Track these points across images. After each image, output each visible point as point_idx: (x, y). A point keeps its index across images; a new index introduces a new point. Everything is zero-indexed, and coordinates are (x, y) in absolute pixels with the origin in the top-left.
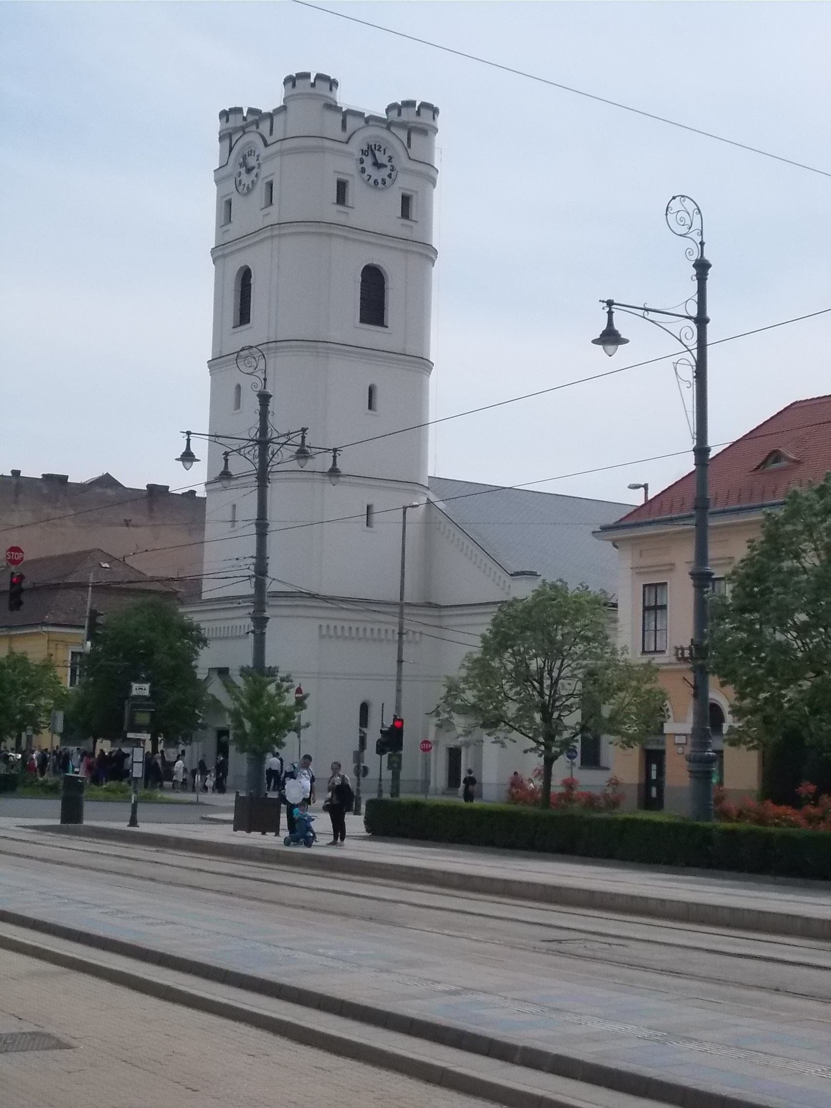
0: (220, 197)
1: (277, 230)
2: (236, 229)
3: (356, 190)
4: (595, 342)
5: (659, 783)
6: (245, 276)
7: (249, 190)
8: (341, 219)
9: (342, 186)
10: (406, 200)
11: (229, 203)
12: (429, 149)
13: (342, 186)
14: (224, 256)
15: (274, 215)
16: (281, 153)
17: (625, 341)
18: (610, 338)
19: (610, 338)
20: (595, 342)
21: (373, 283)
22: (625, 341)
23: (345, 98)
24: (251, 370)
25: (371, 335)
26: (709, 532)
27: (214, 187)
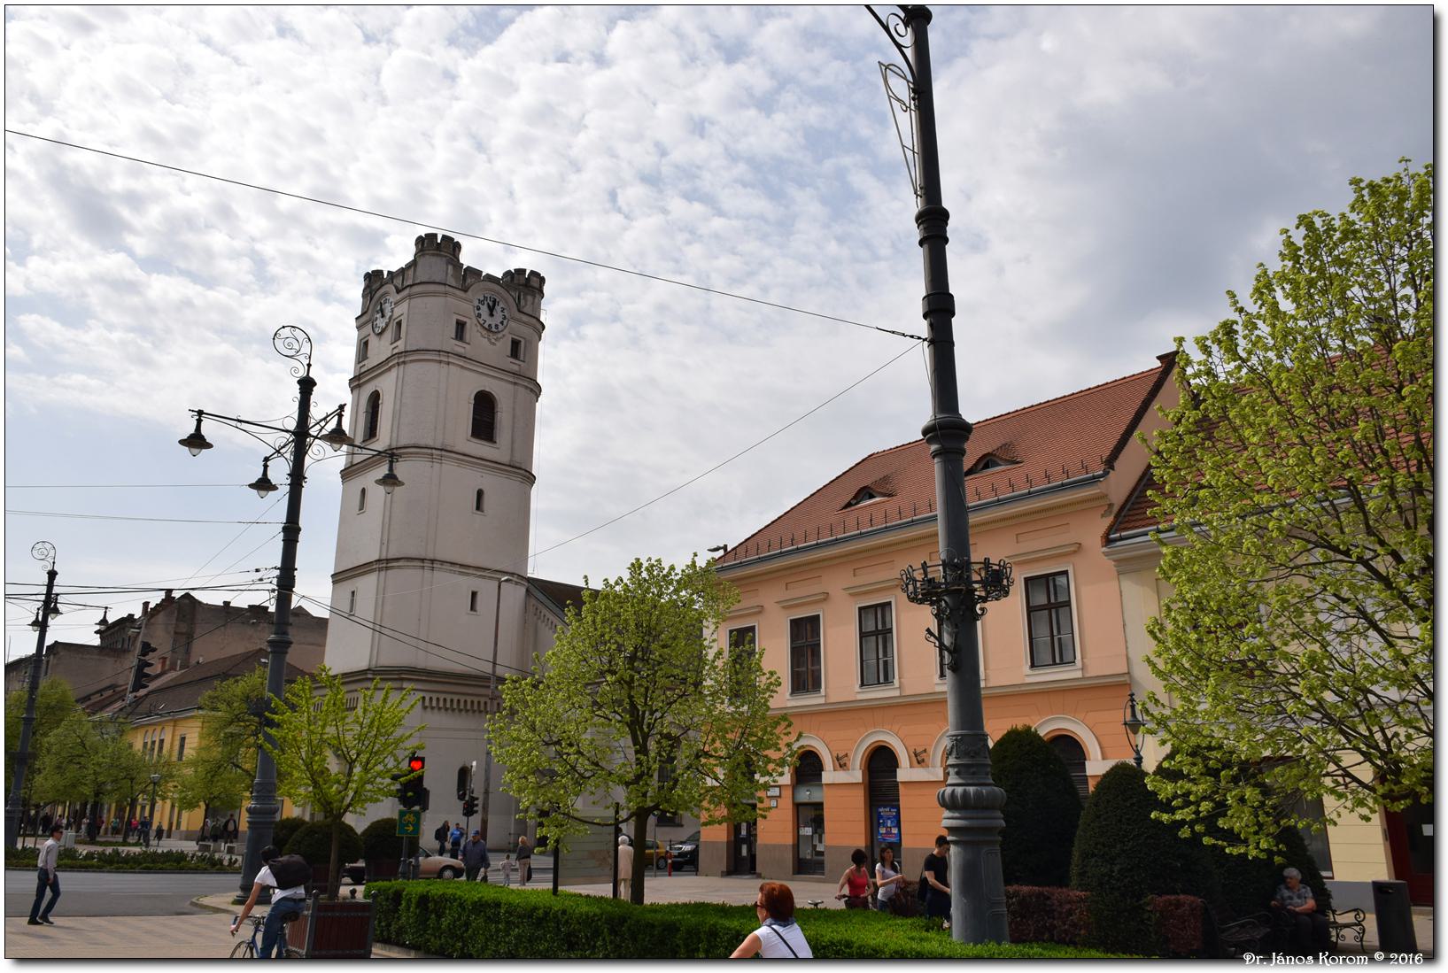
0: (360, 341)
1: (399, 359)
2: (372, 362)
3: (472, 331)
4: (182, 442)
5: (751, 840)
6: (375, 399)
7: (380, 334)
8: (460, 351)
9: (461, 326)
10: (515, 344)
11: (366, 343)
12: (537, 308)
13: (461, 326)
14: (359, 386)
15: (401, 345)
16: (410, 296)
17: (209, 446)
18: (196, 441)
19: (196, 441)
20: (182, 442)
21: (484, 406)
22: (209, 446)
23: (466, 259)
24: (292, 353)
25: (480, 448)
26: (985, 705)
27: (355, 333)
